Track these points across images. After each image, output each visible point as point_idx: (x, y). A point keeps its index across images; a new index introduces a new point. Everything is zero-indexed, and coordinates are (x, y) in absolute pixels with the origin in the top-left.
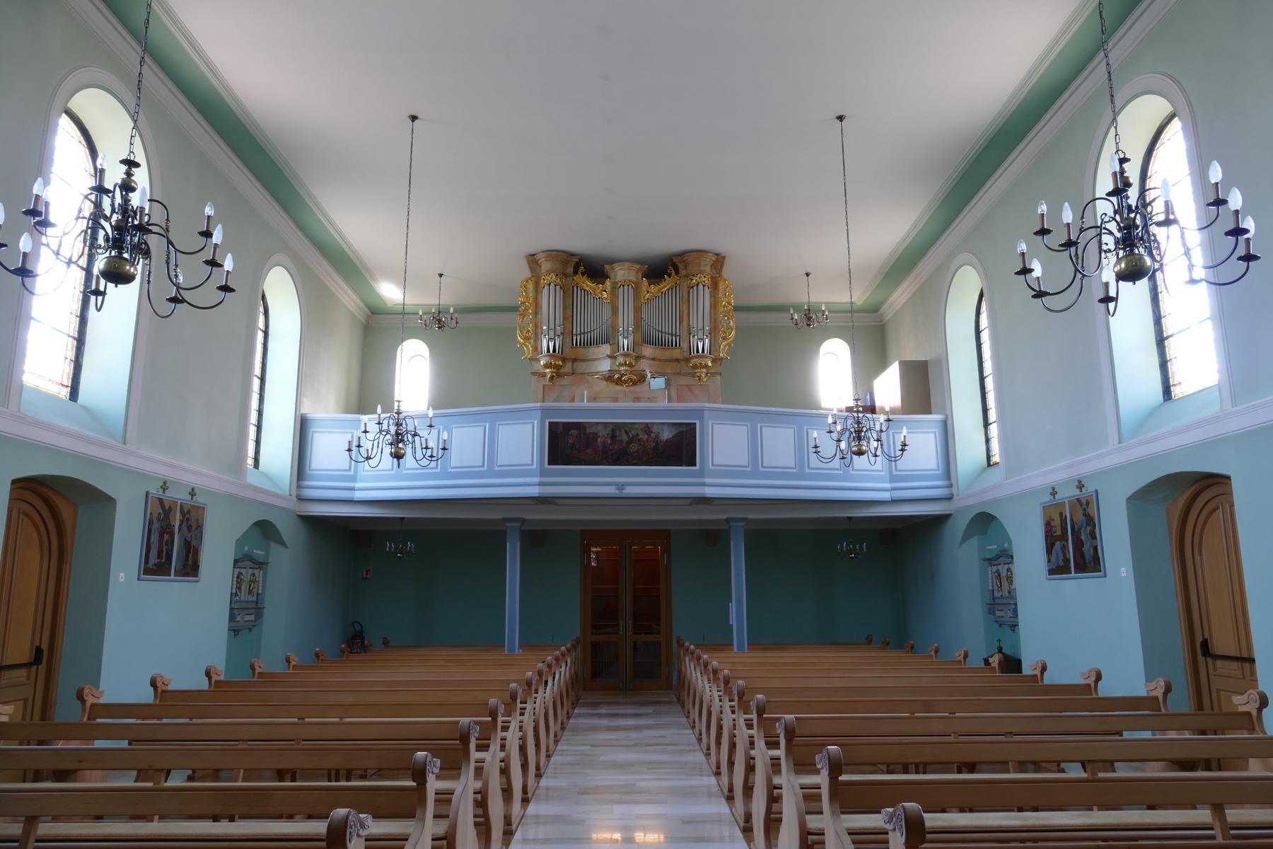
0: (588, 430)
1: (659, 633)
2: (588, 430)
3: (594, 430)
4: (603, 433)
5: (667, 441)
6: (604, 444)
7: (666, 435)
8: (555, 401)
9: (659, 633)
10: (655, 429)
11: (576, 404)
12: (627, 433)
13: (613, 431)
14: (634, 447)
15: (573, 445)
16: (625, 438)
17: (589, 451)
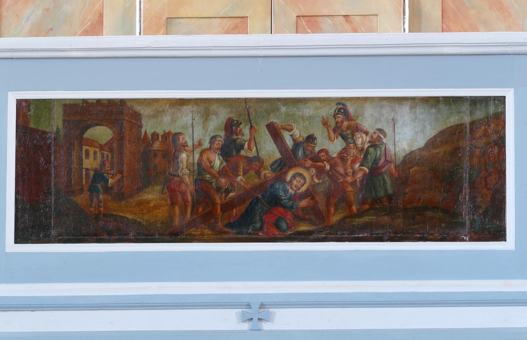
0: (148, 127)
1: (502, 100)
2: (148, 127)
3: (164, 124)
4: (198, 134)
5: (410, 160)
6: (201, 170)
7: (407, 137)
8: (38, 31)
9: (502, 100)
10: (368, 121)
11: (109, 41)
12: (275, 132)
13: (231, 126)
14: (299, 181)
15: (99, 176)
16: (269, 150)
17: (152, 195)
